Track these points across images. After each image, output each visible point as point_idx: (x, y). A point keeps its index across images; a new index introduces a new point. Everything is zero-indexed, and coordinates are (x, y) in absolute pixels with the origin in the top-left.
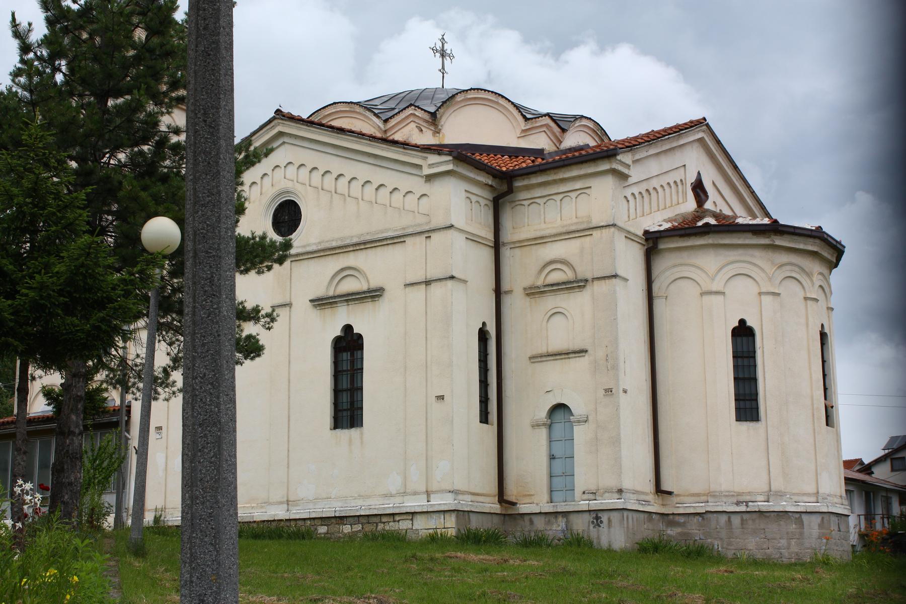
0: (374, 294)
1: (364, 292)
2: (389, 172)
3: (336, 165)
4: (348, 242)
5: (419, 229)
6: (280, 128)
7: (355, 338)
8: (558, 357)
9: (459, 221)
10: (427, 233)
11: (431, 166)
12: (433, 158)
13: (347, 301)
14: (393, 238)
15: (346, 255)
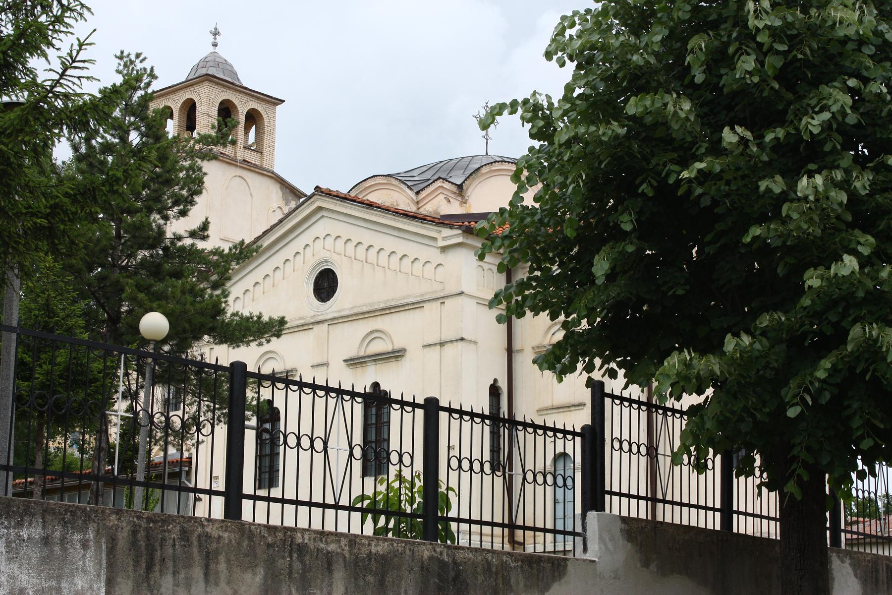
0: (397, 355)
1: (389, 353)
2: (411, 243)
3: (367, 236)
4: (376, 307)
5: (435, 296)
6: (318, 204)
7: (382, 394)
8: (561, 410)
9: (469, 287)
10: (442, 299)
11: (444, 238)
12: (447, 232)
13: (374, 360)
14: (413, 304)
15: (374, 319)
